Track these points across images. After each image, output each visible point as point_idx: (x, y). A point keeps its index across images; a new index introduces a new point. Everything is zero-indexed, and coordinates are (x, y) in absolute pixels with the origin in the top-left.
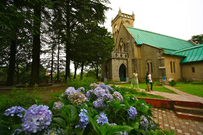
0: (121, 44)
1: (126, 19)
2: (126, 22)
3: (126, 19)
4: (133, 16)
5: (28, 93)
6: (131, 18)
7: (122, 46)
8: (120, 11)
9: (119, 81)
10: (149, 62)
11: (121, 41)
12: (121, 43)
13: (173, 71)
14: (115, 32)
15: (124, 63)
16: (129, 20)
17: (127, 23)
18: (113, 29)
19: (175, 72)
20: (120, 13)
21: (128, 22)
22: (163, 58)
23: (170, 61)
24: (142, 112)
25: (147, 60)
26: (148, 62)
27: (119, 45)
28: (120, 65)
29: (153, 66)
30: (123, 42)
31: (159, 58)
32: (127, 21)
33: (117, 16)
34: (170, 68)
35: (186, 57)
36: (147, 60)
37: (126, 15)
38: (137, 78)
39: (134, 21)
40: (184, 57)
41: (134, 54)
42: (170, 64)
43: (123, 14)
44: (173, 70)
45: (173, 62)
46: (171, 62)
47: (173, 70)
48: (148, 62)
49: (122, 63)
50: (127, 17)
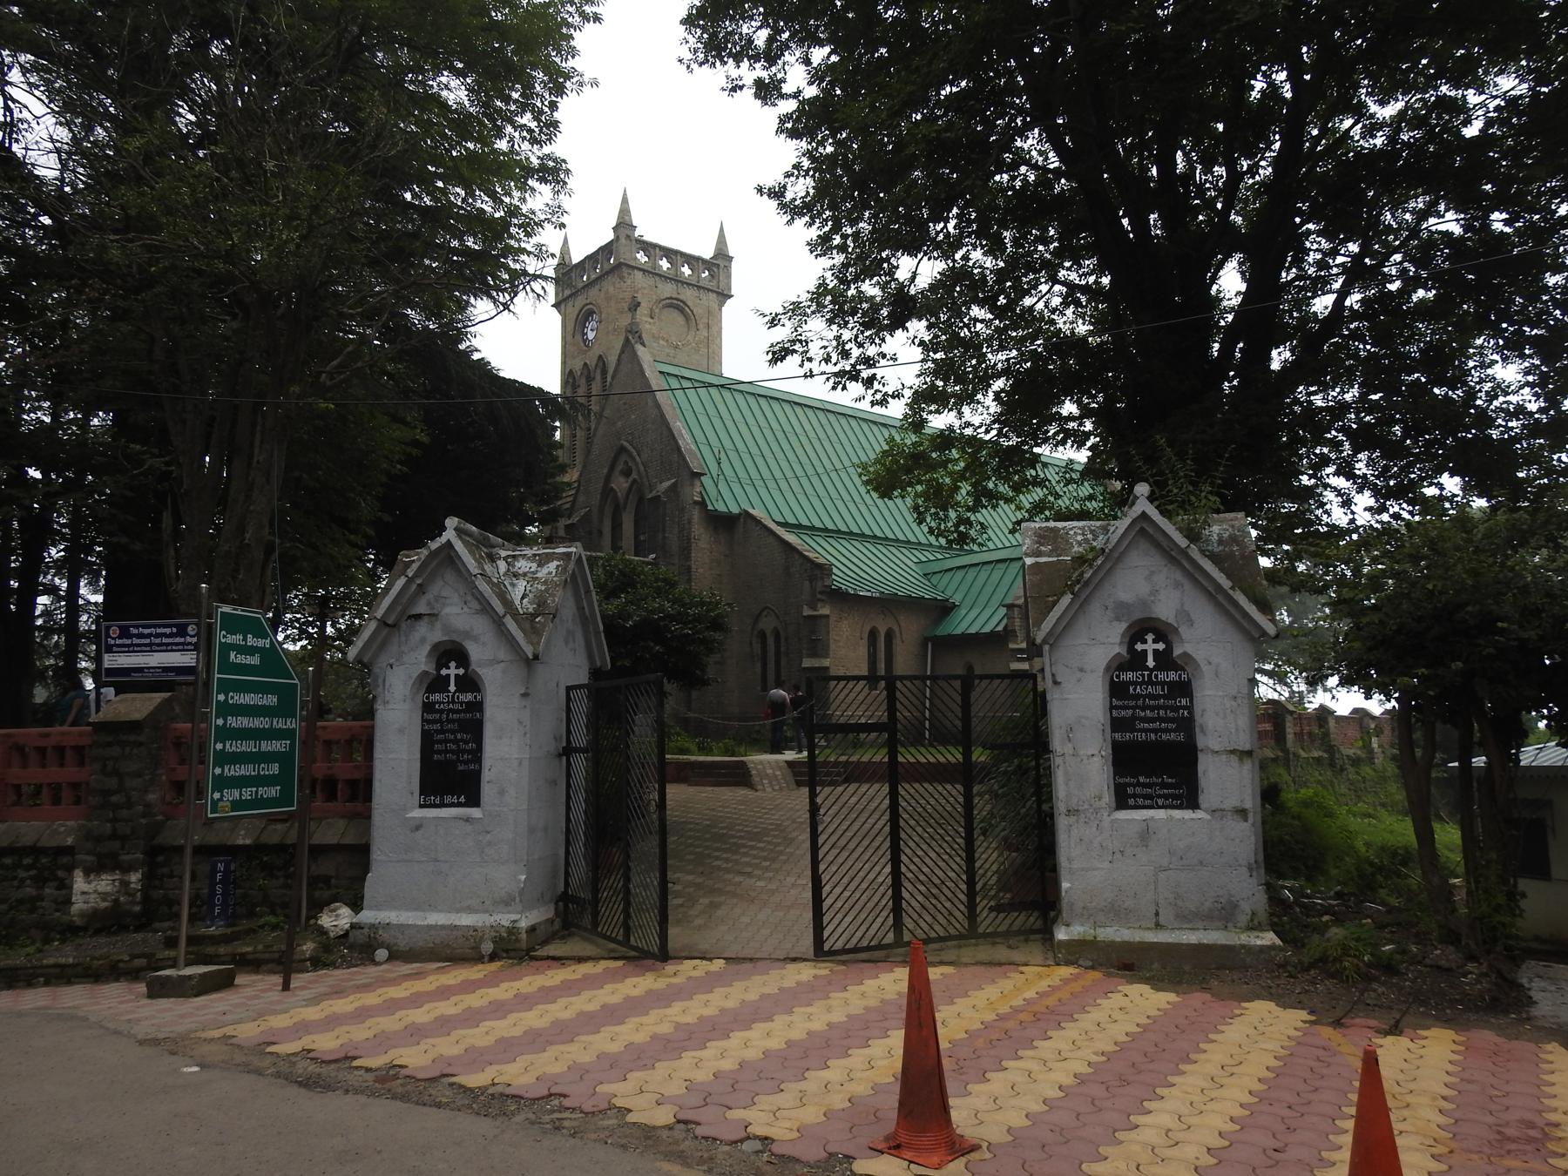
0: (620, 484)
1: (668, 290)
3: (668, 290)
4: (720, 262)
7: (622, 501)
8: (624, 225)
9: (312, 842)
10: (768, 624)
11: (620, 466)
12: (622, 479)
14: (585, 364)
16: (688, 295)
17: (676, 315)
18: (569, 338)
20: (628, 237)
21: (682, 311)
22: (825, 610)
23: (867, 628)
25: (760, 614)
26: (761, 625)
27: (607, 492)
29: (783, 649)
30: (634, 475)
31: (807, 612)
32: (678, 306)
33: (601, 249)
35: (954, 606)
36: (760, 614)
37: (669, 253)
38: (883, 682)
39: (722, 304)
40: (944, 609)
41: (689, 568)
42: (865, 641)
43: (648, 247)
45: (883, 639)
46: (873, 634)
48: (761, 625)
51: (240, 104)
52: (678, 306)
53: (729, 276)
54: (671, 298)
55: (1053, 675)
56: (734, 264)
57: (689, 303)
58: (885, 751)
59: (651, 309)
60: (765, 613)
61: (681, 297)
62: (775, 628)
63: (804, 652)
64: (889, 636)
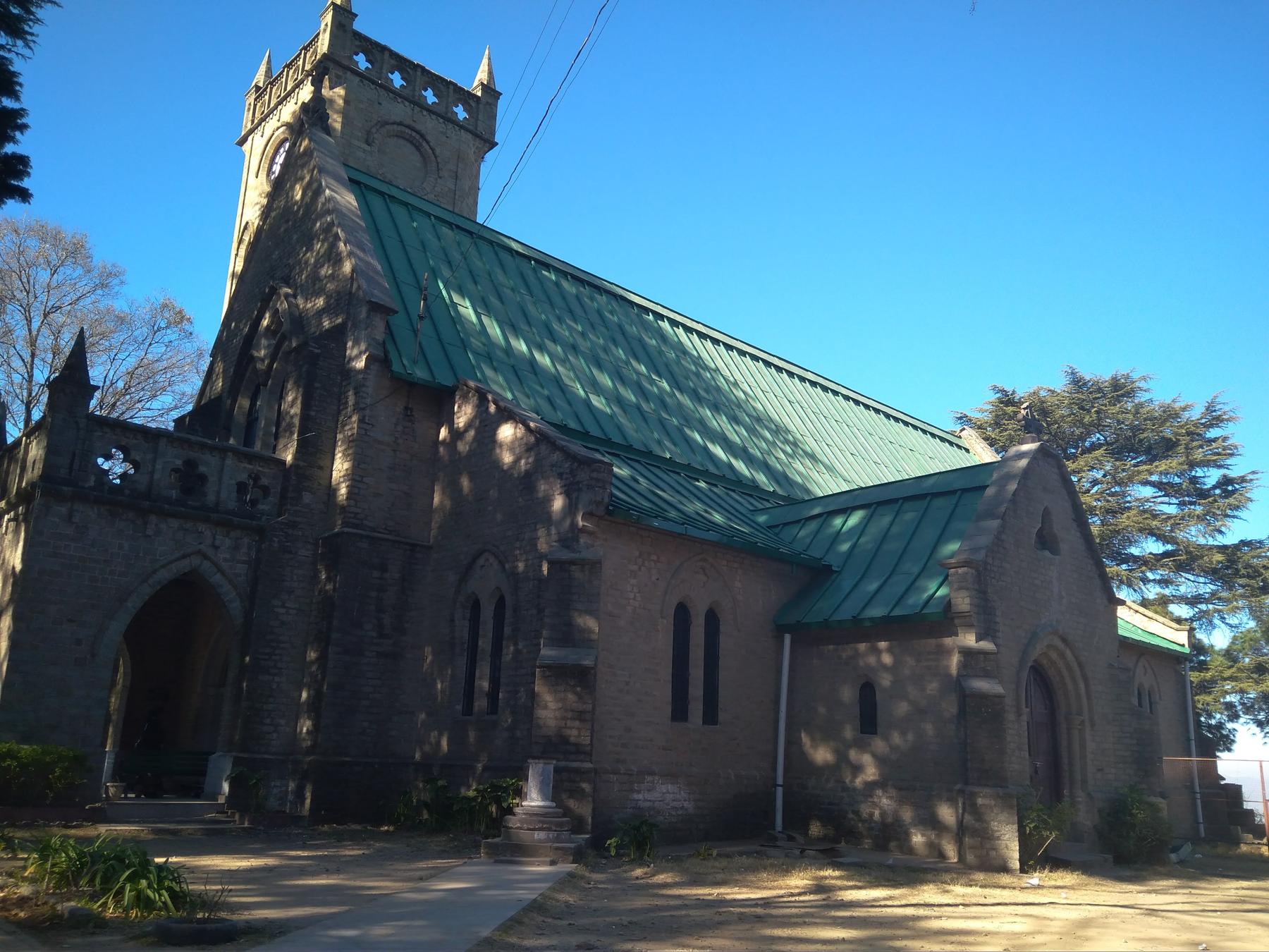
1: (400, 111)
2: (400, 136)
3: (400, 111)
5: (137, 933)
6: (461, 113)
13: (696, 710)
15: (206, 565)
16: (429, 125)
17: (408, 149)
19: (722, 716)
21: (418, 148)
24: (1248, 810)
28: (146, 591)
29: (507, 630)
32: (416, 139)
34: (666, 672)
37: (404, 65)
44: (696, 690)
46: (682, 615)
47: (696, 690)
49: (185, 565)
50: (441, 110)
51: (233, 324)
52: (416, 139)
53: (493, 117)
54: (400, 124)
55: (1137, 612)
56: (501, 103)
57: (429, 138)
58: (589, 731)
59: (369, 133)
60: (481, 561)
61: (419, 127)
62: (498, 588)
63: (545, 633)
64: (712, 619)
